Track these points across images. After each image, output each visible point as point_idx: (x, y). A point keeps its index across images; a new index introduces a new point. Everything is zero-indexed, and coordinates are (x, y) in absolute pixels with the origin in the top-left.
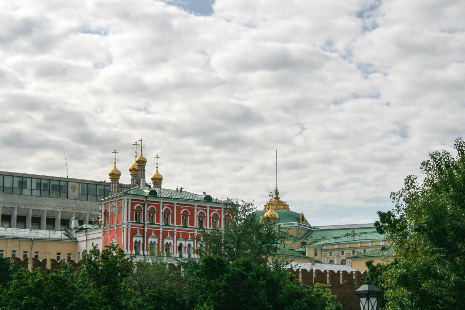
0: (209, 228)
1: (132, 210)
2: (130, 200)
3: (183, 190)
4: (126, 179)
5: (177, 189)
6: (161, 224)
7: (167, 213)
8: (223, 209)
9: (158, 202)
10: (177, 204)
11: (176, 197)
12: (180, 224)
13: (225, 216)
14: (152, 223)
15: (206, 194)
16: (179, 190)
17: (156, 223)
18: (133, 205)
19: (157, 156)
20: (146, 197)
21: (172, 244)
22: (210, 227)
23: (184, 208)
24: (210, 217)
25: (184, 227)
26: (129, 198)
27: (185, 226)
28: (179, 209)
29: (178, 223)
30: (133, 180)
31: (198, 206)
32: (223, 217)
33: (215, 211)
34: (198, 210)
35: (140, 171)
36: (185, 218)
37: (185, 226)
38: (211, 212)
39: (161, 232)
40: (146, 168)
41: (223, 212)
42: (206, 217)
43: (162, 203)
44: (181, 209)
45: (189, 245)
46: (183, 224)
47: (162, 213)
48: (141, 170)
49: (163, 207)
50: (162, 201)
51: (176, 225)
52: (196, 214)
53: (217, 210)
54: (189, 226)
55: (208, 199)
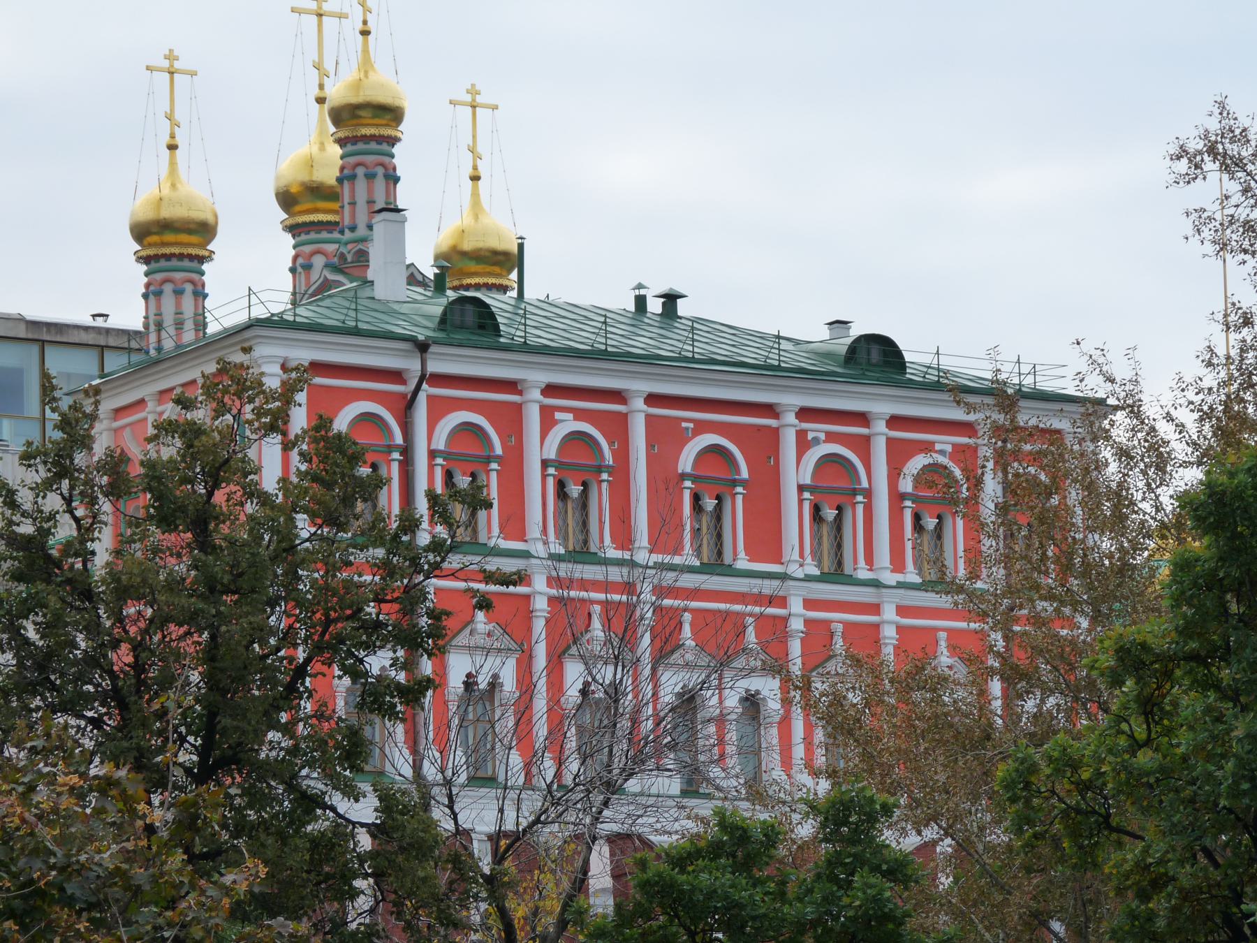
0: (890, 578)
3: (683, 308)
4: (252, 273)
5: (641, 302)
6: (539, 549)
7: (577, 471)
9: (511, 386)
10: (652, 399)
11: (642, 343)
12: (677, 550)
13: (1006, 486)
15: (856, 331)
16: (655, 306)
19: (473, 91)
20: (423, 348)
22: (898, 564)
23: (702, 427)
24: (897, 498)
25: (705, 569)
27: (717, 565)
28: (665, 438)
29: (665, 537)
30: (308, 267)
31: (805, 413)
33: (927, 447)
34: (803, 443)
35: (361, 184)
36: (709, 504)
37: (717, 565)
38: (898, 454)
39: (797, 625)
40: (402, 157)
42: (868, 493)
43: (536, 394)
44: (682, 440)
45: (752, 702)
46: (698, 552)
47: (545, 464)
48: (370, 177)
49: (548, 421)
50: (537, 376)
51: (642, 557)
52: (796, 472)
53: (945, 442)
54: (743, 563)
55: (876, 357)
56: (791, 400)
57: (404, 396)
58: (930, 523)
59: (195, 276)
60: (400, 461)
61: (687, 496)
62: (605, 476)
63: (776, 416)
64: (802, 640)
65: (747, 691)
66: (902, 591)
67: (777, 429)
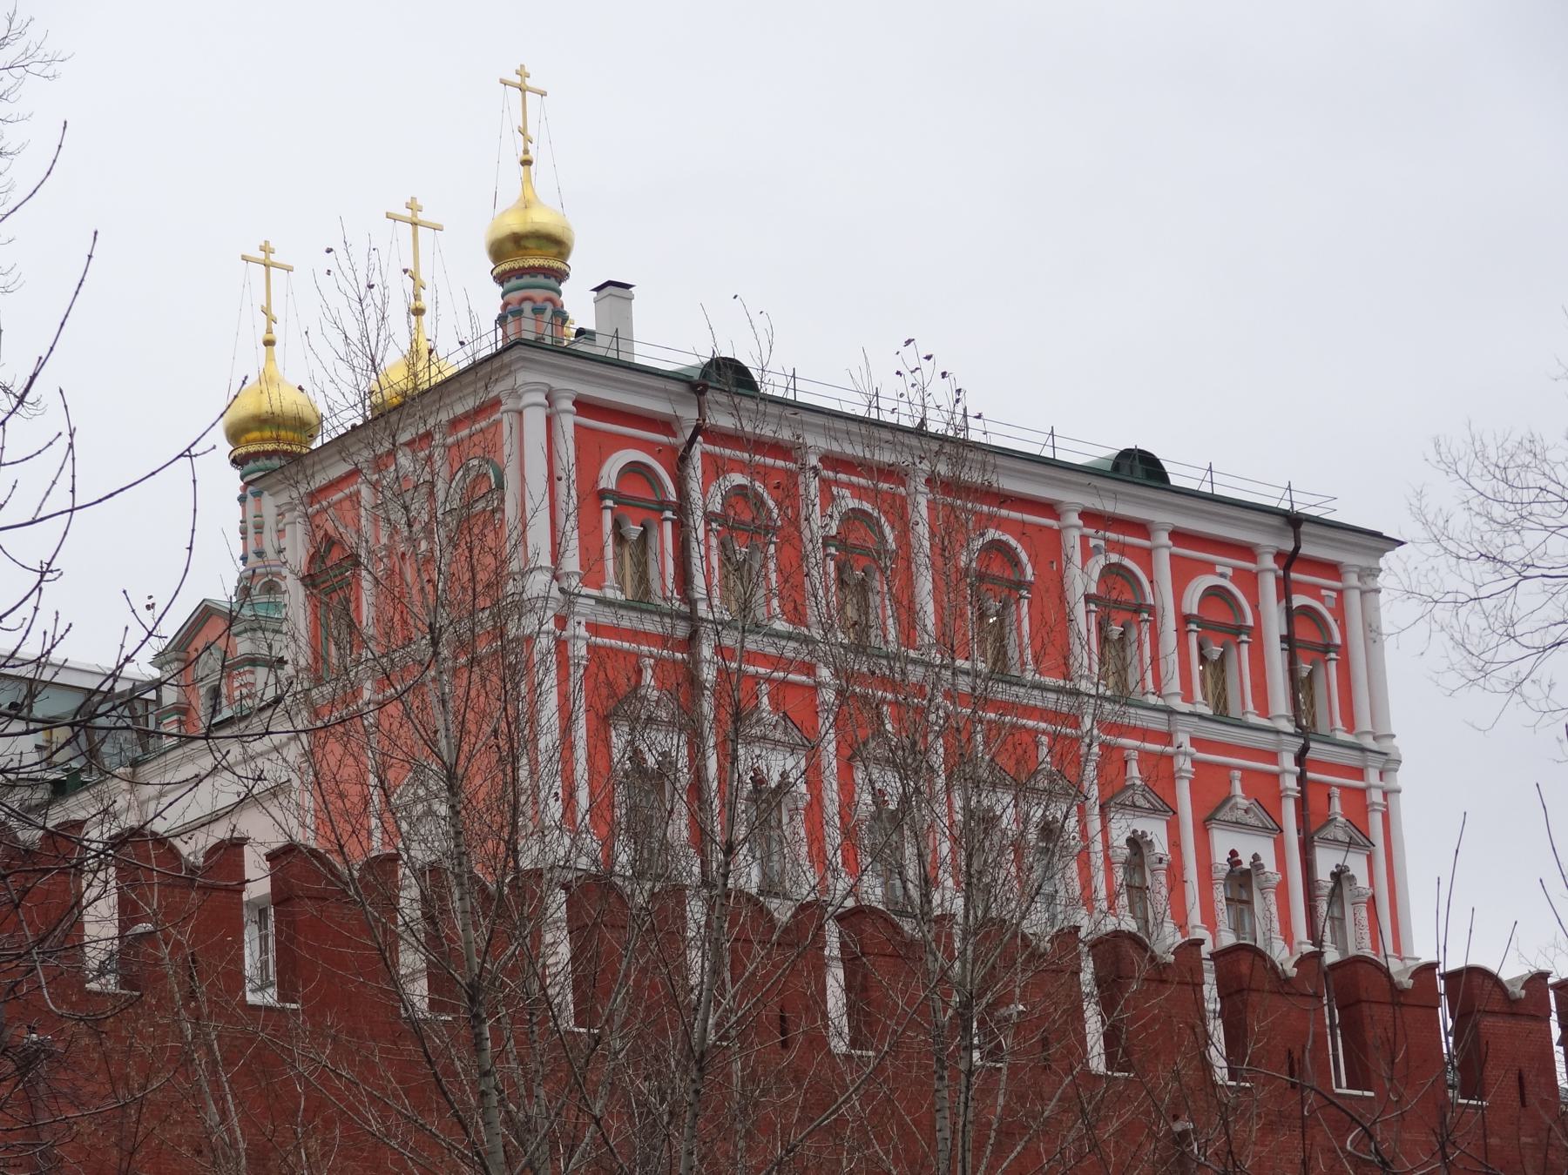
0: (1178, 704)
1: (593, 497)
2: (567, 404)
8: (1268, 562)
13: (1290, 614)
14: (746, 621)
17: (1253, 719)
18: (591, 450)
21: (1269, 863)
26: (557, 383)
31: (1089, 517)
32: (1275, 625)
33: (1209, 568)
41: (1269, 586)
45: (1137, 843)
49: (828, 498)
53: (1226, 564)
56: (1074, 499)
57: (673, 449)
58: (634, 531)
59: (553, 295)
60: (673, 521)
61: (607, 518)
62: (668, 514)
63: (1147, 536)
64: (1192, 782)
65: (1135, 832)
66: (1196, 720)
67: (1059, 532)
